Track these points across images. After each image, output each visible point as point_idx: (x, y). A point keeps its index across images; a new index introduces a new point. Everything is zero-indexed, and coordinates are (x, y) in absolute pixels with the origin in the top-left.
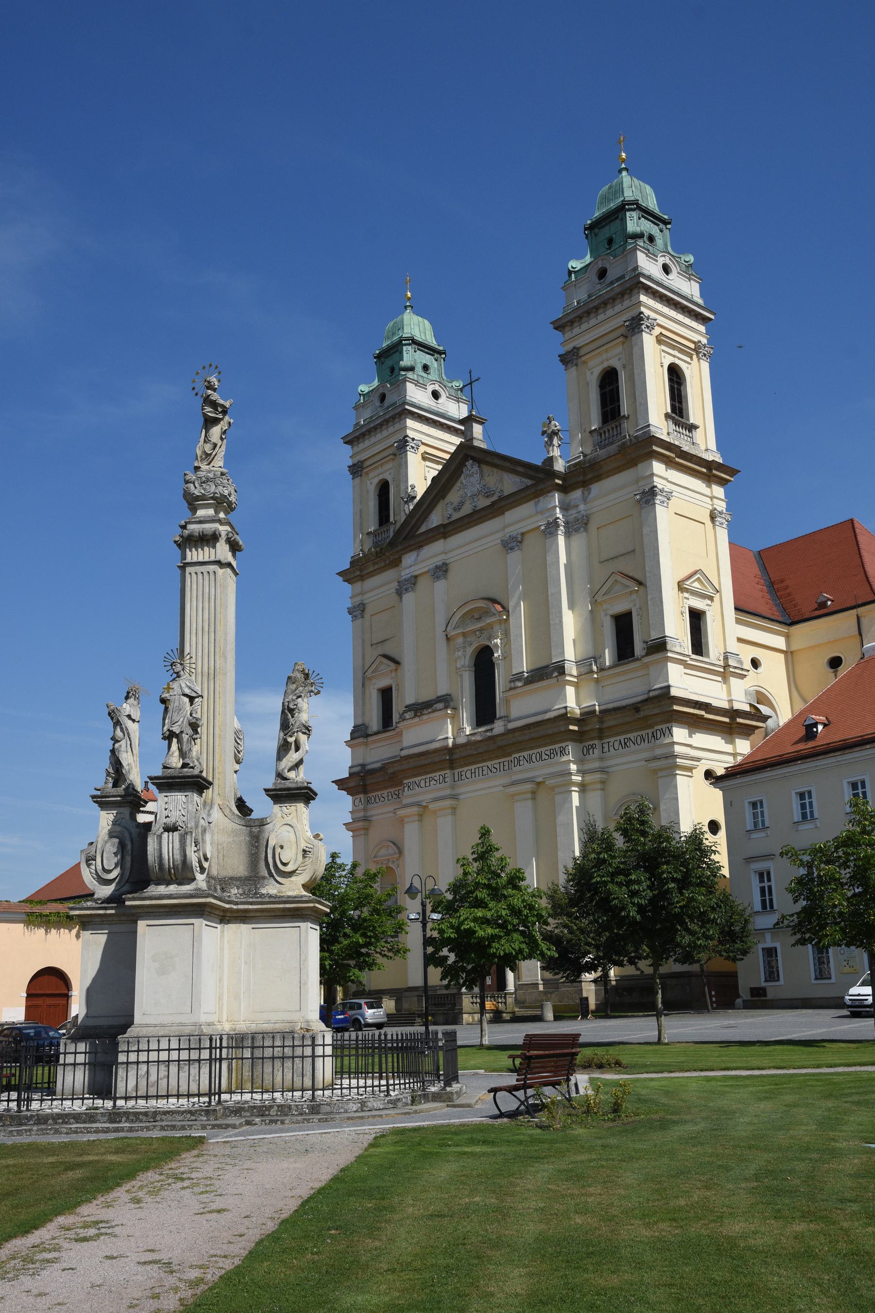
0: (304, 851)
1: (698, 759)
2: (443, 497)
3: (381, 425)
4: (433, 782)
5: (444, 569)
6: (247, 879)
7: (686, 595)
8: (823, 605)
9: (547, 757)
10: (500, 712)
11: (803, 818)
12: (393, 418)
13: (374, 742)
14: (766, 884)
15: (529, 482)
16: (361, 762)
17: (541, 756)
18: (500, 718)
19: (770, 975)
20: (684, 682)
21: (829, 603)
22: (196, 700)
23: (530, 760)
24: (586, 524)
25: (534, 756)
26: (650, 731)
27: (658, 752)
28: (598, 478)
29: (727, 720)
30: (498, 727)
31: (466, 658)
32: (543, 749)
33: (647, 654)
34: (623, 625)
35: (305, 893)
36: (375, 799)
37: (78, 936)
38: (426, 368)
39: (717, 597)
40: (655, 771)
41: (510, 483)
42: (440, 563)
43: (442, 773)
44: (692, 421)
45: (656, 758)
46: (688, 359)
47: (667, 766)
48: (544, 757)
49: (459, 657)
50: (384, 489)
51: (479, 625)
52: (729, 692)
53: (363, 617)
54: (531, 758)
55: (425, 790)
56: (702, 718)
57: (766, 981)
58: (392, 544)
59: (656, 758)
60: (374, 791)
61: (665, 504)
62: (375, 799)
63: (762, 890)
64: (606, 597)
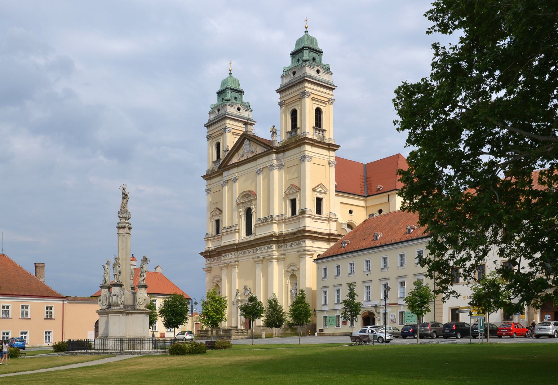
1: (314, 251)
2: (237, 152)
3: (218, 121)
7: (315, 193)
8: (379, 190)
12: (222, 119)
14: (369, 291)
15: (266, 150)
27: (301, 249)
28: (288, 150)
29: (327, 237)
37: (395, 122)
38: (236, 98)
39: (328, 193)
40: (300, 255)
41: (259, 150)
44: (324, 128)
45: (300, 251)
46: (324, 105)
50: (218, 145)
55: (227, 258)
56: (316, 237)
59: (300, 251)
63: (367, 292)
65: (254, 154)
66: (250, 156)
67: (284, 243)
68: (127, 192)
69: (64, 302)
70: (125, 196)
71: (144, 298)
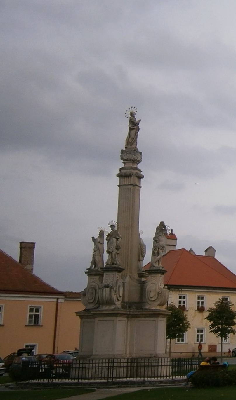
0: (158, 293)
22: (119, 239)
68: (137, 118)
69: (60, 301)
70: (134, 126)
71: (158, 291)
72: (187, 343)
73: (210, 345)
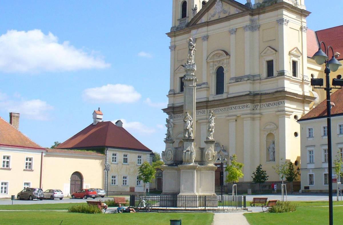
1: (292, 112)
2: (208, 11)
4: (200, 113)
5: (207, 37)
6: (201, 161)
9: (241, 108)
10: (225, 90)
11: (324, 135)
13: (177, 96)
14: (311, 155)
15: (241, 11)
16: (172, 103)
17: (239, 107)
18: (225, 93)
19: (311, 183)
20: (290, 87)
21: (338, 56)
23: (235, 108)
24: (259, 28)
25: (237, 107)
26: (277, 102)
27: (280, 109)
30: (224, 96)
31: (213, 70)
32: (240, 105)
33: (278, 76)
34: (270, 65)
35: (214, 165)
36: (177, 117)
42: (206, 35)
43: (204, 110)
47: (283, 114)
48: (241, 108)
49: (211, 70)
51: (219, 59)
52: (303, 90)
53: (175, 50)
54: (236, 107)
57: (309, 184)
58: (188, 25)
59: (229, 116)
60: (177, 114)
61: (286, 25)
62: (177, 117)
63: (310, 156)
64: (265, 54)
65: (227, 15)
66: (223, 16)
67: (260, 102)
72: (117, 185)
73: (131, 187)
